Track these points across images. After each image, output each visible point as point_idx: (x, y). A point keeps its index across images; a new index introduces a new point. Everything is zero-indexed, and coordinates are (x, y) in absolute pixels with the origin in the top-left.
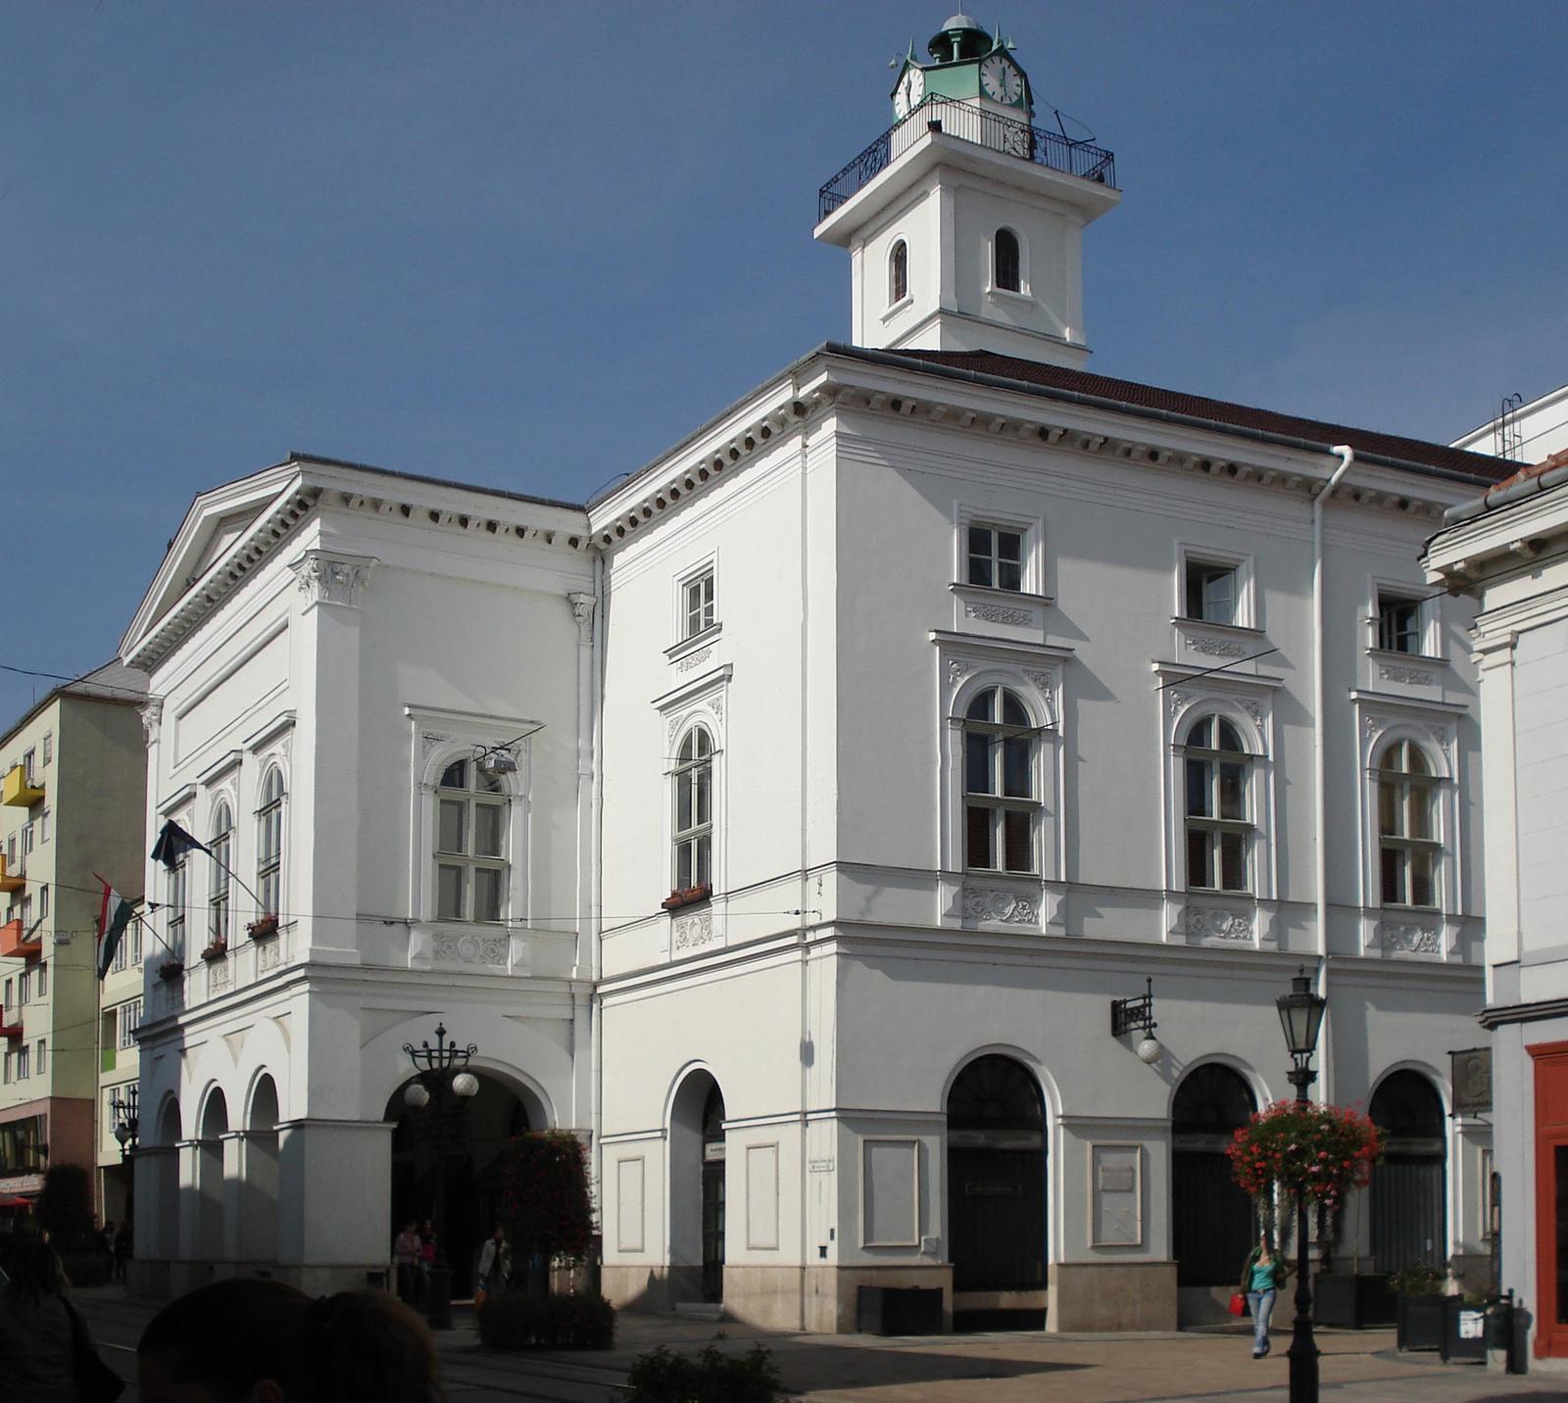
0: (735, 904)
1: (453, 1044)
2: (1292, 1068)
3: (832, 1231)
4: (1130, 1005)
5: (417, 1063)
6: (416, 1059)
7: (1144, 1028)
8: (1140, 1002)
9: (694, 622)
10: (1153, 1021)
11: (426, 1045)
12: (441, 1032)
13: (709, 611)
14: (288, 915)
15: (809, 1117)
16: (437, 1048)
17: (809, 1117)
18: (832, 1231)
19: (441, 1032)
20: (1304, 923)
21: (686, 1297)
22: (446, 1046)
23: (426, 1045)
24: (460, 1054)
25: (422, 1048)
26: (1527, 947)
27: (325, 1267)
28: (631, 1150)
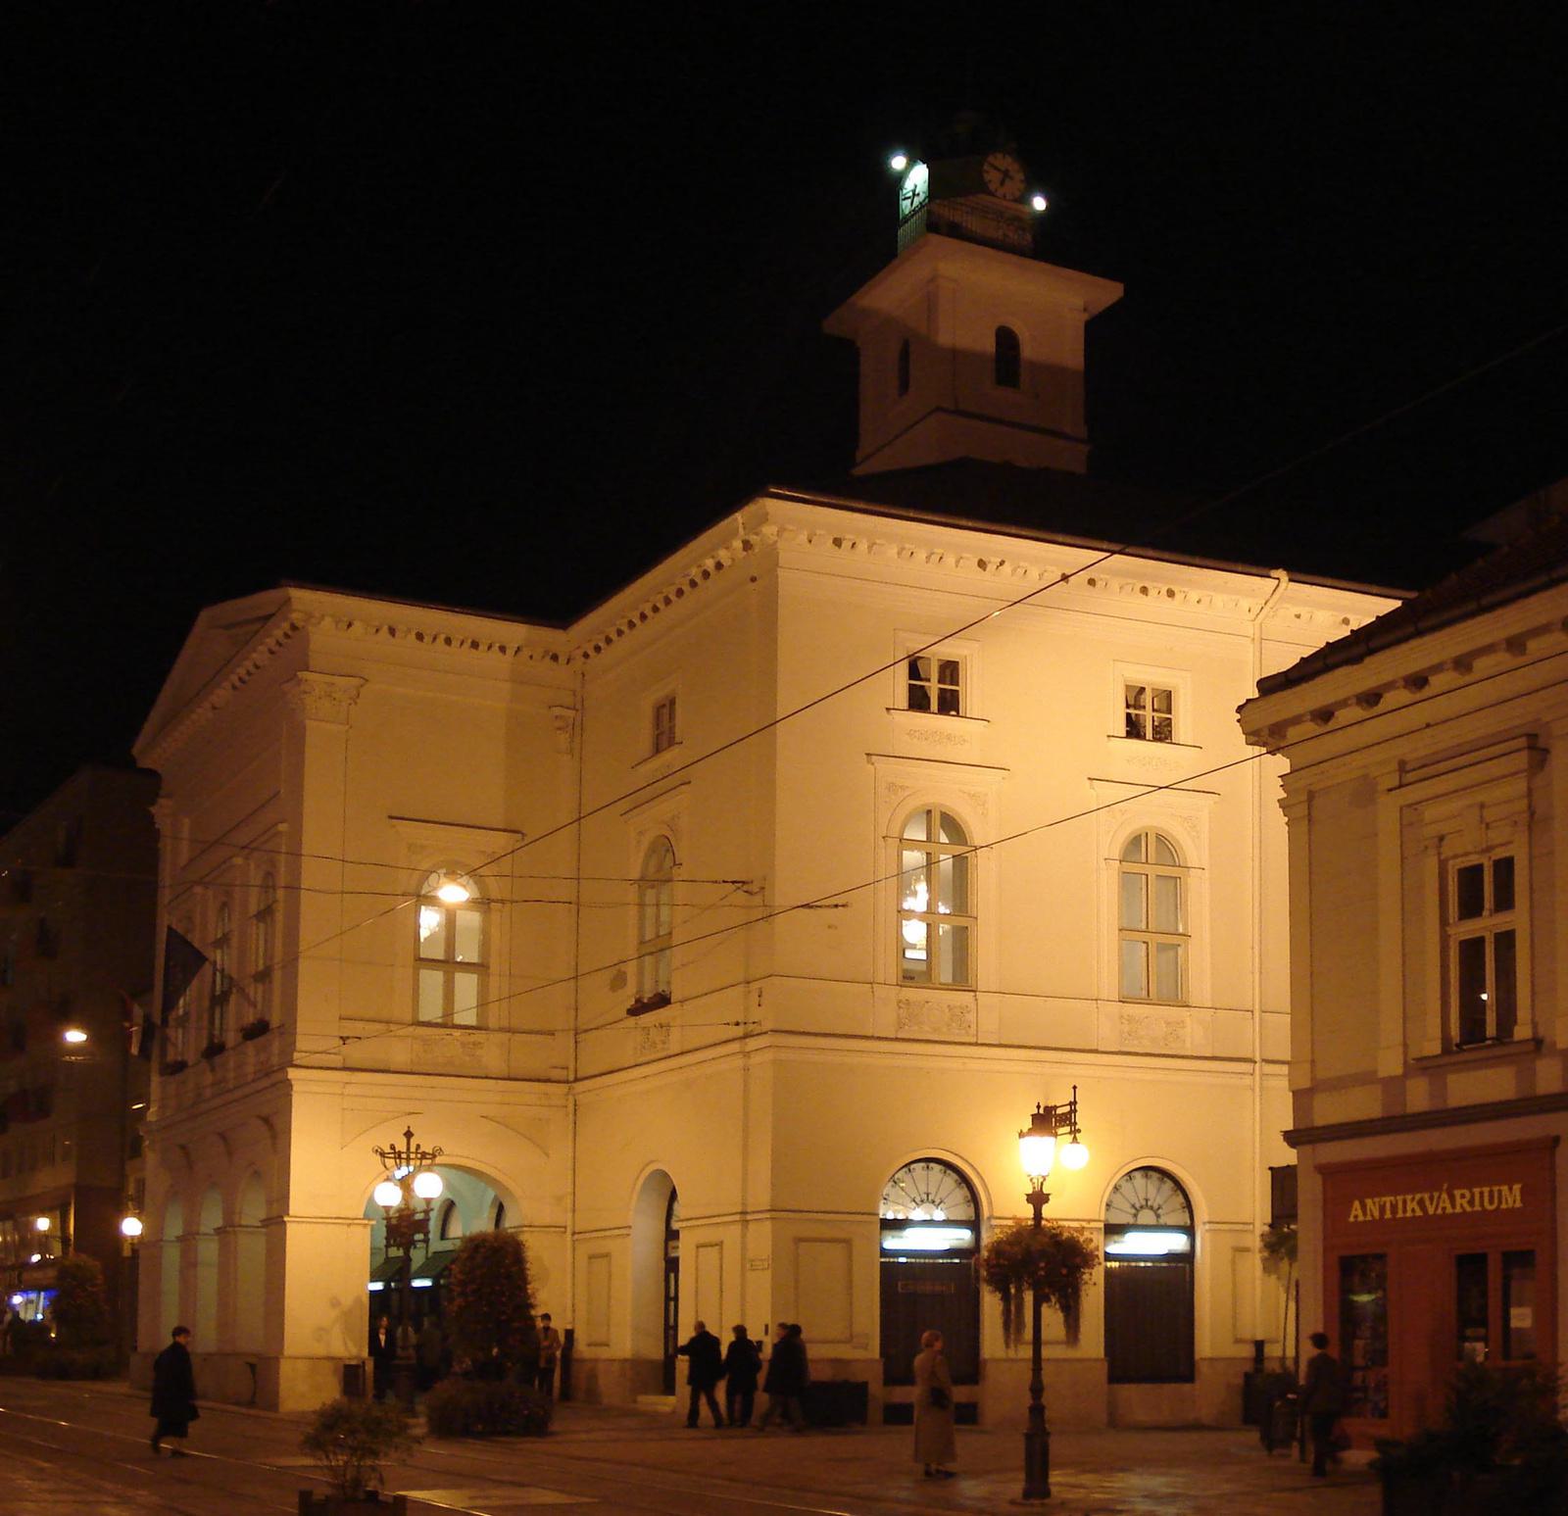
0: (688, 1006)
1: (418, 1146)
2: (1030, 1192)
3: (767, 1326)
4: (1059, 1111)
5: (387, 1164)
6: (386, 1160)
7: (1070, 1133)
8: (1067, 1109)
9: (658, 737)
10: (1077, 1127)
11: (393, 1147)
12: (409, 1135)
13: (672, 729)
14: (341, 960)
15: (749, 1217)
16: (405, 1150)
17: (749, 1217)
18: (767, 1326)
19: (409, 1135)
20: (127, 1252)
21: (645, 1390)
22: (413, 1149)
23: (393, 1147)
24: (428, 1156)
25: (390, 1151)
26: (1321, 1074)
27: (302, 1358)
28: (711, 1235)
